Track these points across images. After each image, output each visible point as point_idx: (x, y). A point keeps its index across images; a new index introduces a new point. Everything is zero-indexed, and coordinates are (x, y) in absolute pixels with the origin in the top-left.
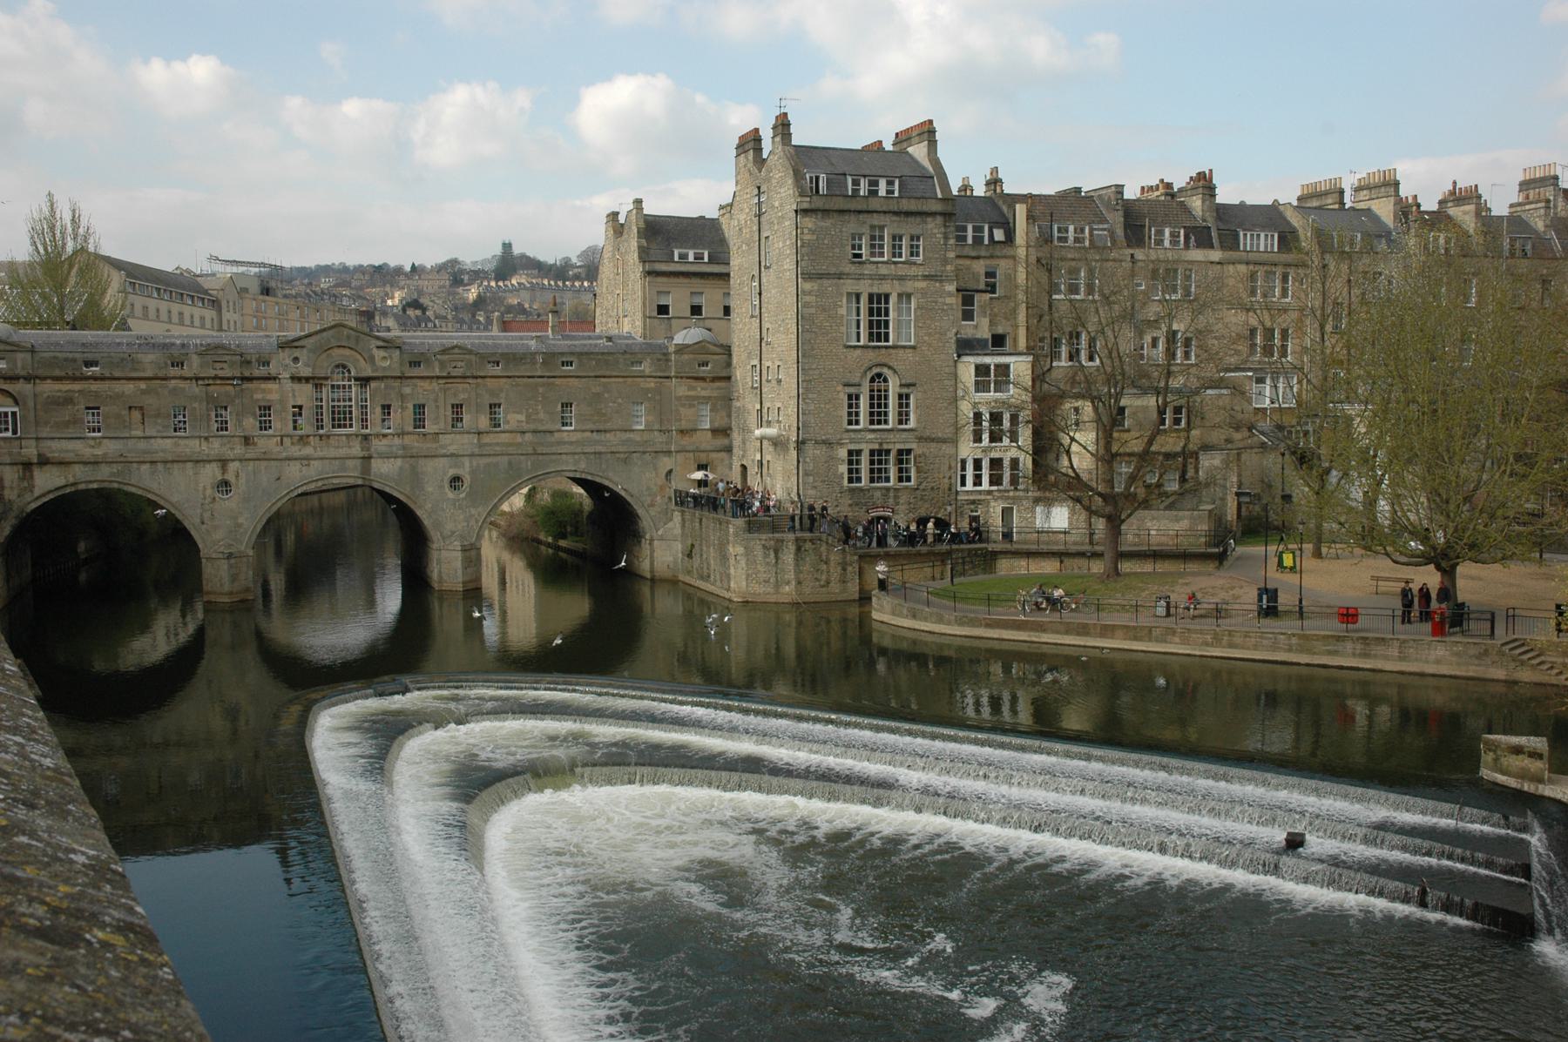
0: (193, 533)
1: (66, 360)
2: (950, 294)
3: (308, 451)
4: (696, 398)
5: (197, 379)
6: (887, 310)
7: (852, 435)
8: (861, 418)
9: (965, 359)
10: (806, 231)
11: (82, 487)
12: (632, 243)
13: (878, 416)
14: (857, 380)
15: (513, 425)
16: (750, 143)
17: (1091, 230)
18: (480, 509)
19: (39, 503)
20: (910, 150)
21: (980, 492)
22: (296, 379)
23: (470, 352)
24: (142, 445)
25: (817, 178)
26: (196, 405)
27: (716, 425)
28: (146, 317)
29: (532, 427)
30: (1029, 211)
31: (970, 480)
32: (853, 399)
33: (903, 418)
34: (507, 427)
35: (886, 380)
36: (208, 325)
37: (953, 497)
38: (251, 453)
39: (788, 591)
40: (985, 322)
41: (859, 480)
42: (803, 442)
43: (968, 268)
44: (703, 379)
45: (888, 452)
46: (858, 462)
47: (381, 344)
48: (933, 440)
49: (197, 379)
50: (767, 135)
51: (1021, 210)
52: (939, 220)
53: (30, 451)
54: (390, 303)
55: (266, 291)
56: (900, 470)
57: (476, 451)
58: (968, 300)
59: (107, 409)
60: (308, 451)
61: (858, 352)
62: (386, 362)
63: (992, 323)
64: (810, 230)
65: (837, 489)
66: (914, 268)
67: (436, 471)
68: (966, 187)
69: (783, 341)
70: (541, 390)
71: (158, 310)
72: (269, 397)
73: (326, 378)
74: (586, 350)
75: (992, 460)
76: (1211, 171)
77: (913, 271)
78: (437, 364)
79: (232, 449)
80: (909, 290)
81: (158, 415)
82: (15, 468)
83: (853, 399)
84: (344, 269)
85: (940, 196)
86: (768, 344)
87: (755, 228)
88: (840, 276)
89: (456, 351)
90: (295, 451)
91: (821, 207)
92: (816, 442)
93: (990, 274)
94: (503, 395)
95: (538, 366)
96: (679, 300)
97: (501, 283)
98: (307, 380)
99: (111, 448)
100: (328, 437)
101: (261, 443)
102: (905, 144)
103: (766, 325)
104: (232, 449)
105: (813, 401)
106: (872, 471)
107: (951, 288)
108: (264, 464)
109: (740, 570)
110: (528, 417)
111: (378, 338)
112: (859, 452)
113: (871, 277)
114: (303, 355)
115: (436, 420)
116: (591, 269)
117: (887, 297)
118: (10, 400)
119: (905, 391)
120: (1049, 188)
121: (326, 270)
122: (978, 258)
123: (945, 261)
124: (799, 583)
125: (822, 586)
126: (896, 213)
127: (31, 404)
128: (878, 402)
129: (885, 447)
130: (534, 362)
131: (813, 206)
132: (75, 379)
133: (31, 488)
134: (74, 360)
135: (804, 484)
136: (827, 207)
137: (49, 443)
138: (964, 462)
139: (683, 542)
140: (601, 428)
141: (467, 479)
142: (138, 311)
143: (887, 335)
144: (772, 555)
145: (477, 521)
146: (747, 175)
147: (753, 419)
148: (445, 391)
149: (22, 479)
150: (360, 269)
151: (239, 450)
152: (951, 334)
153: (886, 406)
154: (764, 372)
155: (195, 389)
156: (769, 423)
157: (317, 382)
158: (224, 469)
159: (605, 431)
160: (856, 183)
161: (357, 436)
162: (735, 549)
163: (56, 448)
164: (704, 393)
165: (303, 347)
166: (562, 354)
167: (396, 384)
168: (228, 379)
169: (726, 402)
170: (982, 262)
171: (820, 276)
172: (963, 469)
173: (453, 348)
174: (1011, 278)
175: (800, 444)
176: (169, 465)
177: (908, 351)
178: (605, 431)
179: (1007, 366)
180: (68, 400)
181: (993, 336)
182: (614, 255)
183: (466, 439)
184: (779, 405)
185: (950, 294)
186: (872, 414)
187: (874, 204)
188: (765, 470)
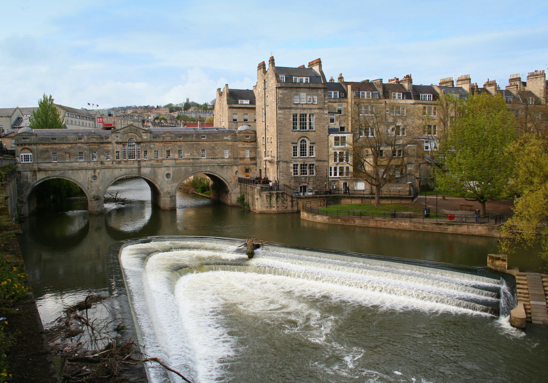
0: (85, 192)
1: (46, 138)
2: (326, 114)
3: (121, 166)
4: (245, 148)
5: (86, 143)
6: (306, 119)
7: (295, 159)
8: (307, 154)
9: (331, 135)
11: (51, 178)
12: (225, 98)
13: (303, 153)
14: (296, 142)
15: (186, 157)
16: (262, 66)
18: (176, 184)
19: (38, 183)
20: (313, 68)
21: (336, 178)
22: (117, 143)
24: (70, 165)
25: (283, 77)
26: (86, 152)
27: (252, 156)
28: (72, 124)
29: (192, 157)
30: (352, 87)
32: (295, 148)
33: (311, 153)
34: (184, 158)
35: (305, 142)
37: (327, 179)
39: (274, 209)
41: (297, 174)
42: (279, 162)
43: (332, 106)
45: (306, 165)
46: (297, 168)
47: (144, 131)
48: (321, 161)
49: (86, 143)
51: (349, 87)
52: (322, 90)
53: (36, 167)
54: (150, 118)
55: (110, 115)
56: (310, 171)
57: (175, 165)
59: (59, 153)
61: (296, 133)
62: (145, 137)
63: (340, 123)
64: (281, 94)
65: (290, 177)
66: (315, 106)
67: (162, 172)
68: (332, 80)
69: (272, 130)
70: (195, 146)
71: (76, 122)
72: (109, 149)
73: (127, 143)
75: (340, 167)
79: (97, 165)
80: (313, 113)
81: (74, 155)
82: (31, 172)
83: (295, 148)
84: (136, 108)
85: (323, 82)
86: (268, 130)
87: (264, 93)
88: (291, 108)
89: (168, 133)
90: (117, 165)
92: (283, 162)
94: (183, 147)
95: (194, 138)
96: (239, 116)
97: (186, 111)
98: (121, 143)
99: (60, 165)
100: (127, 161)
101: (106, 163)
102: (312, 66)
103: (267, 124)
104: (97, 165)
105: (282, 148)
106: (301, 171)
107: (326, 112)
108: (107, 170)
109: (258, 203)
110: (191, 154)
111: (143, 129)
112: (297, 165)
113: (301, 109)
114: (119, 135)
115: (162, 156)
116: (208, 109)
117: (306, 115)
118: (29, 151)
119: (312, 145)
121: (129, 108)
122: (336, 102)
123: (325, 103)
124: (278, 207)
126: (309, 88)
127: (36, 152)
128: (303, 148)
129: (305, 163)
131: (282, 86)
132: (49, 144)
133: (36, 178)
134: (49, 138)
135: (279, 175)
136: (286, 86)
137: (41, 164)
138: (331, 168)
142: (70, 122)
143: (306, 127)
144: (269, 198)
145: (175, 188)
147: (263, 155)
148: (164, 146)
149: (33, 176)
151: (100, 166)
152: (326, 127)
153: (306, 150)
154: (267, 139)
155: (85, 146)
157: (123, 143)
158: (95, 172)
159: (216, 158)
163: (44, 166)
164: (248, 146)
166: (202, 134)
168: (96, 143)
169: (255, 149)
170: (337, 104)
172: (331, 170)
173: (167, 132)
174: (346, 109)
175: (278, 162)
176: (78, 171)
178: (216, 158)
179: (345, 137)
180: (47, 151)
182: (219, 102)
184: (271, 150)
185: (326, 114)
186: (301, 153)
187: (302, 85)
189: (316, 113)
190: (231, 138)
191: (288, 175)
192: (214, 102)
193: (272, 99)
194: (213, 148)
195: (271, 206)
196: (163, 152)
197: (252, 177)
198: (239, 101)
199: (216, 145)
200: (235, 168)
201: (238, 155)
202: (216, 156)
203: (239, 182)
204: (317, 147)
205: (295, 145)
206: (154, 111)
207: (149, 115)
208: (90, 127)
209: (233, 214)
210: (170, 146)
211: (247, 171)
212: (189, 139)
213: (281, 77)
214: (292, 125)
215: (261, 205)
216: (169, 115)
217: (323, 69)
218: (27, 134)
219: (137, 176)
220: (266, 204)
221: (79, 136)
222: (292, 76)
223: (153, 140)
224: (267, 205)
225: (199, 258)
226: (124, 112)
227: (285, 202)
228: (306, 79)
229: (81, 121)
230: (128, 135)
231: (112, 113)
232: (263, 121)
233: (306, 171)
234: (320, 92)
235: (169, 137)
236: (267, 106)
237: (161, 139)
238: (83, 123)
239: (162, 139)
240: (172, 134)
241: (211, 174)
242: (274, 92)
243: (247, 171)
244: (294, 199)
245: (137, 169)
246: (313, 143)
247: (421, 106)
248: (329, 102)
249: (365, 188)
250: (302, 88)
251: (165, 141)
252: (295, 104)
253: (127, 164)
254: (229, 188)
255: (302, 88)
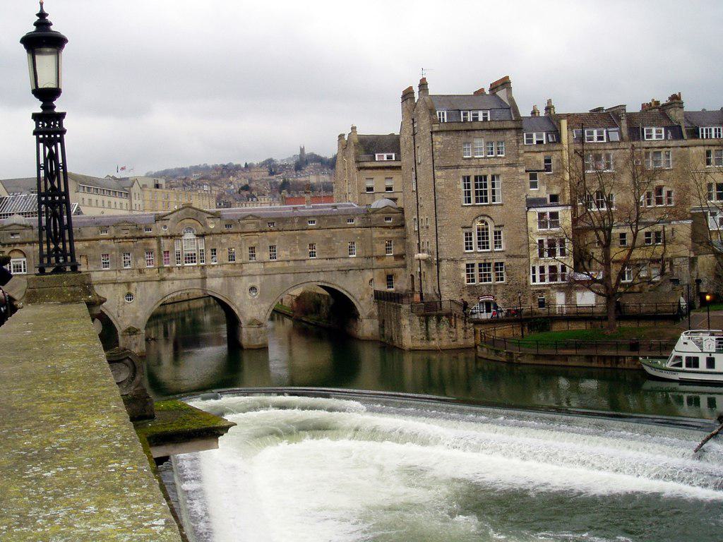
2: (522, 174)
3: (172, 275)
7: (468, 255)
10: (437, 143)
12: (352, 151)
13: (483, 244)
14: (469, 225)
16: (408, 95)
17: (607, 132)
21: (544, 285)
23: (258, 218)
25: (443, 113)
26: (114, 253)
28: (90, 205)
29: (293, 258)
30: (568, 123)
31: (538, 278)
33: (497, 244)
34: (279, 259)
35: (486, 224)
36: (124, 207)
38: (142, 277)
40: (544, 188)
41: (473, 281)
43: (534, 158)
44: (388, 227)
45: (489, 265)
46: (472, 271)
47: (209, 216)
50: (416, 90)
51: (564, 123)
55: (157, 186)
56: (497, 274)
57: (263, 272)
58: (533, 177)
60: (172, 275)
61: (470, 209)
66: (500, 160)
74: (322, 214)
76: (680, 93)
77: (500, 162)
78: (240, 226)
79: (133, 276)
80: (497, 172)
81: (94, 259)
87: (412, 142)
88: (458, 167)
91: (445, 129)
92: (448, 260)
93: (548, 161)
94: (277, 241)
96: (378, 181)
101: (147, 272)
103: (420, 196)
104: (133, 276)
106: (481, 275)
107: (522, 170)
108: (149, 283)
111: (208, 213)
112: (473, 265)
113: (476, 167)
114: (168, 224)
116: (331, 164)
117: (485, 177)
118: (22, 255)
119: (498, 229)
120: (585, 109)
122: (540, 152)
123: (518, 155)
125: (454, 341)
126: (487, 130)
128: (483, 234)
129: (487, 261)
130: (293, 222)
136: (449, 129)
138: (534, 268)
139: (379, 320)
140: (330, 256)
141: (258, 288)
142: (86, 202)
144: (425, 324)
146: (407, 113)
150: (216, 168)
151: (137, 276)
153: (487, 238)
154: (420, 222)
155: (112, 244)
156: (423, 251)
160: (465, 114)
161: (198, 266)
162: (405, 322)
164: (390, 235)
165: (168, 219)
166: (309, 217)
167: (218, 237)
171: (446, 168)
172: (534, 272)
173: (248, 216)
174: (560, 161)
177: (498, 207)
181: (551, 196)
183: (257, 266)
185: (522, 174)
186: (479, 243)
187: (476, 126)
188: (422, 277)
189: (502, 173)
190: (360, 223)
191: (456, 283)
192: (335, 158)
193: (423, 153)
194: (329, 240)
195: (428, 339)
196: (243, 251)
197: (399, 288)
198: (376, 155)
199: (334, 235)
200: (369, 275)
201: (372, 251)
202: (334, 253)
203: (375, 298)
204: (507, 232)
205: (468, 230)
206: (240, 174)
207: (231, 183)
208: (121, 209)
209: (369, 358)
210: (256, 239)
211: (390, 279)
212: (287, 226)
213: (440, 113)
214: (463, 197)
215: (412, 337)
216: (267, 180)
217: (515, 94)
218: (17, 227)
219: (200, 294)
220: (420, 335)
221: (103, 226)
222: (460, 111)
223: (225, 229)
224: (421, 337)
225: (260, 401)
226: (185, 179)
227: (454, 330)
228: (484, 114)
229: (107, 199)
230: (183, 224)
231: (162, 181)
232: (413, 191)
233: (489, 275)
234: (510, 136)
235: (253, 225)
236: (419, 164)
237: (240, 229)
238: (109, 202)
239: (240, 228)
240: (258, 218)
241: (326, 285)
242: (428, 139)
243: (390, 279)
244: (468, 324)
245: (200, 281)
246: (499, 226)
247: (702, 150)
248: (525, 152)
249: (596, 301)
250: (477, 130)
251: (245, 231)
252: (466, 159)
253: (183, 272)
254: (359, 309)
255: (477, 130)
